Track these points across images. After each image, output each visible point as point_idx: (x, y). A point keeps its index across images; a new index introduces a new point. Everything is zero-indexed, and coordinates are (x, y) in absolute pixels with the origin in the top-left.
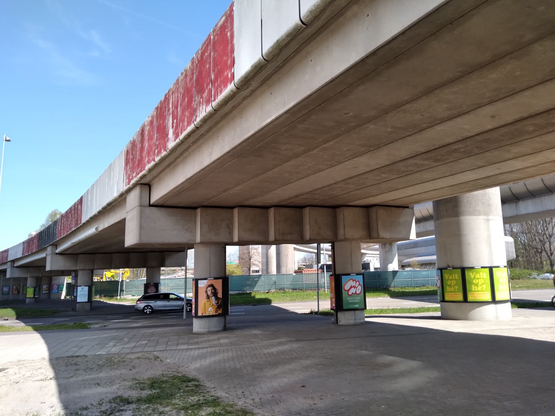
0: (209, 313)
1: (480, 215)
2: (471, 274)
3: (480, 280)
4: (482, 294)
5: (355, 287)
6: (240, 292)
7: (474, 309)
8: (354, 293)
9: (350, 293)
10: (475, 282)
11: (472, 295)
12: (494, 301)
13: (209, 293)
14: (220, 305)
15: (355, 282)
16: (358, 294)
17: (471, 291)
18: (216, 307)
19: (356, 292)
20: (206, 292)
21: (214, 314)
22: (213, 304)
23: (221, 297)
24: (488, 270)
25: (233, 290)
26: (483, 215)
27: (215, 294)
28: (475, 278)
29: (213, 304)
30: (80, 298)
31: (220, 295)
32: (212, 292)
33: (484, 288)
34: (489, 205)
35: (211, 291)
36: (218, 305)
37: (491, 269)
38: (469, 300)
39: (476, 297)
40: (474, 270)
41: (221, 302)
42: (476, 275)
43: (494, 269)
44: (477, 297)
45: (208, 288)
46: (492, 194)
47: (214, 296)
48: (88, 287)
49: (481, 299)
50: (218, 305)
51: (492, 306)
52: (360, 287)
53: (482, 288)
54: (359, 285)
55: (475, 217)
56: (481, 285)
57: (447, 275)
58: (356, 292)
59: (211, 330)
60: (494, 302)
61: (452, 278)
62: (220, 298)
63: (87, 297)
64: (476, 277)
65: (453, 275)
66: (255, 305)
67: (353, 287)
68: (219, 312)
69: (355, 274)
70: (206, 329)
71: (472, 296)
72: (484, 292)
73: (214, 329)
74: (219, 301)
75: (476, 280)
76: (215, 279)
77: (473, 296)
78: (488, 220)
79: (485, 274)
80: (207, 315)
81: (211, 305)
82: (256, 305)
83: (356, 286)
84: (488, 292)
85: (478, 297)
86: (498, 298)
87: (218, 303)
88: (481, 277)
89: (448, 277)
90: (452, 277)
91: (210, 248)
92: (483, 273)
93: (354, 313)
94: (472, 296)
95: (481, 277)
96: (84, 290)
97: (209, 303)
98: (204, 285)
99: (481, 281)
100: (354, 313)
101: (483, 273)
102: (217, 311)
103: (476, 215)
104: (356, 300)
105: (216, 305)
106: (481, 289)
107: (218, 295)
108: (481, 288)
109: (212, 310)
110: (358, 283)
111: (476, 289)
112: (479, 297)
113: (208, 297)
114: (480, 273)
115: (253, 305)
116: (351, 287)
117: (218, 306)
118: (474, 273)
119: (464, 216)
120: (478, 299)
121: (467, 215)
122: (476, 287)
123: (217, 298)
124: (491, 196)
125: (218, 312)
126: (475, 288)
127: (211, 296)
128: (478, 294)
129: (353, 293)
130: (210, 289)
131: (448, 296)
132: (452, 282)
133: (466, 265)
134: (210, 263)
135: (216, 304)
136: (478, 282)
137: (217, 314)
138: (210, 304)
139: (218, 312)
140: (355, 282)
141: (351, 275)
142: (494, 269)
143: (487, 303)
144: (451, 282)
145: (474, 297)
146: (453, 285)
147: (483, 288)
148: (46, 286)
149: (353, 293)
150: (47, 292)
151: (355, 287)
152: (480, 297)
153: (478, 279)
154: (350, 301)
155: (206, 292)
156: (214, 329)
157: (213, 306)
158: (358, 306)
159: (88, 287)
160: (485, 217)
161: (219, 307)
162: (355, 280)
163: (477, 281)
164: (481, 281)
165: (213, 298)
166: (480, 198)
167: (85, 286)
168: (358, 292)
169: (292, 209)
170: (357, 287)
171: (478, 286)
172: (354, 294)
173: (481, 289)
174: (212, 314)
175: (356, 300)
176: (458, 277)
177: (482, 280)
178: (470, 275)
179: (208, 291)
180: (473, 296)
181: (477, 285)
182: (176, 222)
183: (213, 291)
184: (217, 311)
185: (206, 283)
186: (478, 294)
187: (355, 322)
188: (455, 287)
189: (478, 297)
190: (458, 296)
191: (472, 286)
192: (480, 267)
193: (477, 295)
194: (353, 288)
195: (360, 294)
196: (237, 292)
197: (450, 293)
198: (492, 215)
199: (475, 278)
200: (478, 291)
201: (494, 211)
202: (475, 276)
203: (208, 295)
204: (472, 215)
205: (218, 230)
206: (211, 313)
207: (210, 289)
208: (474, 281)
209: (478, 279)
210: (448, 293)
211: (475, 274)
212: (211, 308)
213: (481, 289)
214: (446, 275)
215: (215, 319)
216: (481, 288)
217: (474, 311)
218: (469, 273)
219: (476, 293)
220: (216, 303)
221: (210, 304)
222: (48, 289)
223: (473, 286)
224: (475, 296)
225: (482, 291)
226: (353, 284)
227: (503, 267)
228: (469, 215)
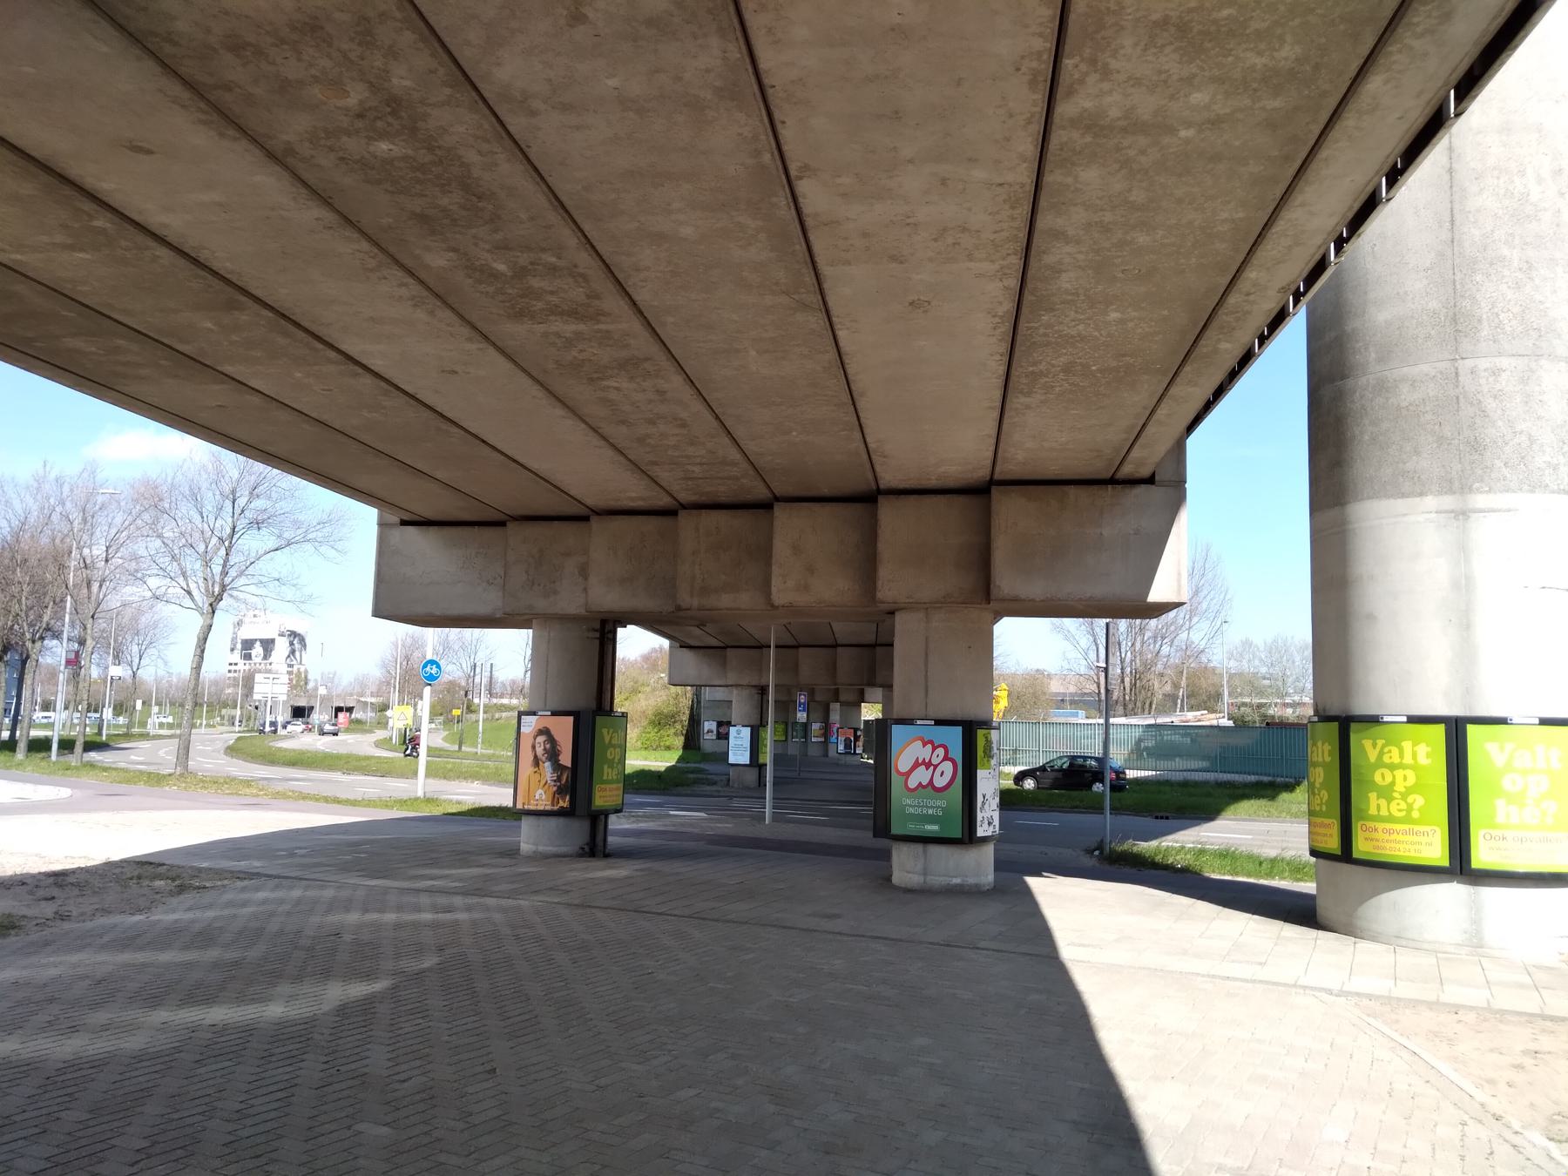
0: (535, 803)
1: (1421, 494)
2: (1367, 744)
3: (1399, 773)
4: (1405, 833)
5: (928, 765)
6: (1266, 779)
7: (1377, 892)
8: (924, 783)
9: (912, 783)
10: (1381, 779)
11: (1367, 834)
12: (1460, 866)
13: (540, 750)
14: (564, 785)
15: (929, 747)
16: (939, 790)
17: (1365, 817)
18: (555, 789)
19: (931, 782)
20: (534, 747)
21: (549, 808)
22: (547, 782)
23: (570, 766)
24: (1439, 731)
25: (1259, 772)
26: (1440, 493)
27: (553, 754)
28: (1380, 764)
29: (547, 782)
30: (735, 754)
31: (566, 759)
32: (545, 749)
33: (1416, 806)
34: (1476, 446)
35: (542, 747)
36: (558, 784)
37: (1456, 730)
38: (1355, 855)
39: (1380, 844)
40: (1377, 729)
41: (568, 777)
42: (1386, 750)
43: (1470, 728)
44: (1386, 844)
45: (537, 736)
46: (1495, 397)
47: (549, 759)
48: (749, 728)
49: (1385, 855)
50: (558, 784)
51: (1453, 892)
52: (948, 767)
53: (1405, 807)
54: (946, 758)
55: (1400, 505)
56: (1404, 796)
57: (1374, 746)
58: (931, 782)
59: (541, 848)
60: (1461, 873)
61: (1396, 760)
62: (566, 767)
63: (748, 754)
64: (1386, 759)
65: (1407, 745)
66: (1162, 818)
67: (924, 762)
68: (561, 804)
69: (933, 723)
70: (530, 846)
71: (1366, 839)
72: (1416, 828)
73: (550, 848)
74: (561, 774)
75: (1386, 772)
76: (554, 714)
77: (1372, 840)
78: (1462, 514)
79: (1422, 750)
80: (532, 808)
81: (543, 782)
82: (1167, 818)
83: (935, 761)
84: (1437, 829)
85: (1388, 845)
86: (1482, 856)
87: (559, 779)
88: (1408, 760)
89: (611, 737)
90: (1401, 756)
91: (549, 632)
92: (1414, 745)
93: (925, 852)
94: (1366, 839)
95: (1408, 760)
96: (741, 735)
97: (537, 775)
98: (531, 729)
99: (1405, 778)
100: (925, 852)
101: (1414, 745)
102: (556, 800)
103: (1403, 496)
104: (932, 807)
105: (553, 783)
106: (1400, 810)
107: (560, 758)
108: (1403, 805)
109: (544, 797)
110: (941, 751)
111: (1384, 812)
112: (1393, 845)
113: (536, 762)
114: (1404, 744)
115: (1157, 818)
116: (916, 765)
117: (559, 787)
118: (1380, 742)
119: (1362, 499)
120: (1388, 852)
121: (1369, 498)
122: (1383, 802)
123: (557, 767)
124: (1490, 404)
125: (559, 805)
126: (1378, 806)
127: (544, 759)
128: (1390, 832)
129: (920, 783)
130: (541, 739)
131: (601, 794)
132: (1399, 779)
133: (1362, 707)
134: (547, 671)
135: (555, 781)
136: (1393, 783)
137: (556, 808)
138: (539, 781)
139: (559, 805)
140: (929, 747)
141: (919, 722)
142: (1470, 728)
143: (1428, 876)
144: (1394, 777)
145: (1377, 843)
146: (1403, 790)
147: (1410, 808)
148: (818, 724)
149: (920, 783)
150: (823, 739)
151: (928, 765)
152: (1397, 846)
153: (1392, 767)
154: (912, 810)
155: (534, 747)
156: (550, 848)
157: (547, 786)
158: (935, 828)
159: (749, 728)
160: (1448, 501)
161: (561, 791)
162: (931, 742)
163: (1389, 779)
164: (1405, 778)
165: (548, 764)
166: (1429, 417)
167: (743, 726)
168: (940, 782)
169: (739, 512)
170: (936, 767)
171: (1390, 799)
172: (924, 787)
173: (1404, 813)
174: (541, 808)
175: (932, 807)
176: (1428, 756)
177: (1411, 774)
178: (1366, 747)
179: (537, 746)
180: (1372, 840)
181: (1387, 793)
182: (464, 563)
183: (548, 746)
184: (556, 800)
185: (533, 724)
186: (1390, 832)
187: (925, 882)
188: (1410, 800)
189: (1401, 846)
190: (1424, 839)
191: (1370, 795)
192: (1405, 719)
193: (1386, 837)
194: (923, 767)
195: (950, 789)
196: (1253, 778)
197: (608, 786)
198: (1490, 491)
199: (1380, 764)
200: (1391, 819)
201: (1505, 471)
202: (1381, 754)
203: (536, 757)
204: (1388, 497)
205: (554, 582)
206: (542, 805)
207: (541, 739)
208: (1377, 778)
209: (1392, 767)
210: (603, 786)
211: (1383, 746)
212: (540, 791)
213: (1400, 810)
214: (605, 731)
215: (553, 822)
216: (1403, 805)
217: (1374, 901)
218: (1364, 742)
219: (1380, 826)
220: (555, 778)
221: (539, 781)
222: (822, 731)
223: (1373, 796)
224: (1377, 840)
225: (1407, 819)
226: (925, 753)
227: (1537, 721)
228: (1376, 496)
